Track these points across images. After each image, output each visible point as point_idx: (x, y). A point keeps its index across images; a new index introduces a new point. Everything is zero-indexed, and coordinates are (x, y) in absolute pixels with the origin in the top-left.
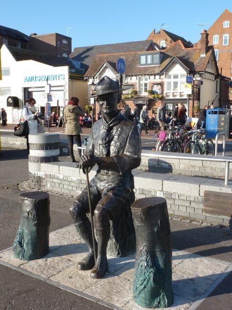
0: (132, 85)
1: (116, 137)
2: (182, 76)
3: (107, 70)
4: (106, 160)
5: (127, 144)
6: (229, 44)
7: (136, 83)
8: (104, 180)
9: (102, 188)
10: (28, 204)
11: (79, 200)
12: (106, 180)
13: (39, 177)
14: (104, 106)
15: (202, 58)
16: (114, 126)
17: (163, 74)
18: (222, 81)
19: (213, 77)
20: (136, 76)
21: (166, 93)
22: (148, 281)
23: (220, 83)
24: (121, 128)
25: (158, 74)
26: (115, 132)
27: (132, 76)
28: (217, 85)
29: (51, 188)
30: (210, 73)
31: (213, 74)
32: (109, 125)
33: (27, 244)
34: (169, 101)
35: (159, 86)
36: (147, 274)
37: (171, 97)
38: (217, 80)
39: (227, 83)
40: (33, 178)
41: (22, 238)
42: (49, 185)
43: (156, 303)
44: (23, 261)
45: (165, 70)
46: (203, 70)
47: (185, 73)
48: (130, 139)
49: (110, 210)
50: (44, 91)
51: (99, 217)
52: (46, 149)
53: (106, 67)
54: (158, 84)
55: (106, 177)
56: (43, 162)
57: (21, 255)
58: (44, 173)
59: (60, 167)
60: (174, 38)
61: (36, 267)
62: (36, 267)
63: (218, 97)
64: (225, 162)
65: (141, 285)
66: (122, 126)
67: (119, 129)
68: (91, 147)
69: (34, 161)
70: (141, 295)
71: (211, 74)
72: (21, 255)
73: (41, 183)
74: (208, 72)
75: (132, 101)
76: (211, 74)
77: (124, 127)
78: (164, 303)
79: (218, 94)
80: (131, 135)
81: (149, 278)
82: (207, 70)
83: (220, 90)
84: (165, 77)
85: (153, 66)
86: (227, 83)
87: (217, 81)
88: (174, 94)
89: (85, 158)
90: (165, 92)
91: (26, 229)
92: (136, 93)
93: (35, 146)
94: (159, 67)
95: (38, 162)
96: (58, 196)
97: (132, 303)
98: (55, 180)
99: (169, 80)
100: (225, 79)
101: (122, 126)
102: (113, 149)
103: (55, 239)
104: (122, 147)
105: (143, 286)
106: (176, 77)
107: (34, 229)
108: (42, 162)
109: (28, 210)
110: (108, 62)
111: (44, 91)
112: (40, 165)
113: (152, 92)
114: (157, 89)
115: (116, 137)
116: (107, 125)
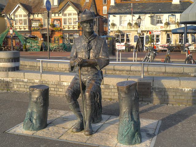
0: (39, 20)
1: (94, 47)
2: (74, 14)
3: (20, 9)
4: (88, 60)
5: (101, 51)
7: (42, 19)
8: (86, 75)
9: (85, 79)
10: (36, 94)
11: (71, 88)
12: (87, 74)
13: (7, 82)
15: (87, 2)
16: (92, 40)
17: (61, 13)
20: (41, 14)
22: (130, 129)
23: (99, 20)
25: (57, 13)
26: (93, 44)
27: (39, 14)
29: (18, 89)
32: (89, 39)
33: (36, 120)
34: (72, 32)
35: (59, 22)
36: (129, 125)
37: (67, 29)
39: (103, 20)
40: (2, 83)
41: (31, 115)
42: (15, 87)
43: (134, 141)
44: (34, 132)
45: (62, 10)
47: (76, 12)
48: (103, 48)
49: (94, 92)
51: (89, 96)
52: (12, 62)
53: (19, 7)
54: (57, 20)
55: (87, 72)
56: (10, 71)
57: (31, 128)
58: (11, 79)
59: (25, 74)
61: (41, 133)
62: (41, 133)
63: (98, 29)
64: (142, 64)
65: (125, 132)
66: (97, 40)
67: (96, 42)
68: (75, 54)
69: (3, 71)
70: (126, 138)
72: (31, 128)
73: (8, 86)
75: (39, 32)
77: (99, 41)
78: (138, 141)
79: (98, 27)
80: (103, 46)
81: (131, 127)
83: (99, 25)
84: (63, 15)
85: (54, 7)
86: (103, 20)
88: (74, 27)
89: (79, 60)
90: (62, 26)
91: (34, 110)
92: (41, 26)
93: (3, 60)
94: (58, 8)
95: (6, 71)
96: (25, 94)
97: (119, 144)
98: (20, 83)
99: (65, 17)
101: (97, 40)
102: (91, 55)
103: (52, 114)
104: (98, 53)
105: (127, 133)
106: (70, 14)
107: (42, 109)
108: (9, 71)
109: (37, 97)
110: (20, 3)
112: (8, 74)
113: (54, 26)
114: (56, 23)
115: (94, 47)
116: (87, 39)
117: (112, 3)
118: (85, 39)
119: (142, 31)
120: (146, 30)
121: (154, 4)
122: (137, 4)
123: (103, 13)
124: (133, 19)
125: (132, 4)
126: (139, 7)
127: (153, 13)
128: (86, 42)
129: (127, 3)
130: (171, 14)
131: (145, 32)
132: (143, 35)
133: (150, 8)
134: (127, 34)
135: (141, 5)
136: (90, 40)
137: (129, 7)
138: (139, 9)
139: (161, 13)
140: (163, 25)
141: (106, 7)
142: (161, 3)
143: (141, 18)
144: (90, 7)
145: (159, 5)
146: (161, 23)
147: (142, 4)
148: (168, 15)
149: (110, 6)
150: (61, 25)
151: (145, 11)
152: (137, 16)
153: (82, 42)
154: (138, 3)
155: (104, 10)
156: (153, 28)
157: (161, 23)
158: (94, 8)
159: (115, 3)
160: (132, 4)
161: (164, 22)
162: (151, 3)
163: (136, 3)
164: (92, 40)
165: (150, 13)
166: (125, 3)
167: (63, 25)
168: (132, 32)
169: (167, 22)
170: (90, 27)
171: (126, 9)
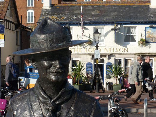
6: (35, 4)
14: (127, 73)
16: (62, 103)
18: (23, 32)
19: (12, 26)
21: (152, 59)
23: (21, 34)
24: (76, 107)
28: (17, 36)
30: (9, 21)
31: (13, 23)
32: (54, 101)
38: (17, 30)
46: (3, 18)
50: (22, 16)
60: (108, 1)
71: (11, 22)
74: (7, 21)
76: (11, 22)
82: (6, 18)
87: (17, 32)
100: (27, 30)
111: (22, 16)
117: (46, 5)
118: (41, 99)
119: (101, 56)
120: (107, 52)
121: (118, 8)
122: (90, 8)
124: (84, 34)
125: (81, 7)
126: (93, 13)
127: (118, 24)
128: (48, 110)
129: (71, 5)
130: (149, 26)
131: (105, 56)
132: (102, 61)
133: (113, 15)
134: (74, 59)
135: (97, 9)
136: (57, 103)
137: (76, 12)
138: (93, 16)
139: (132, 23)
140: (136, 44)
141: (33, 11)
142: (131, 6)
143: (99, 30)
144: (6, 10)
145: (127, 9)
146: (133, 40)
147: (99, 7)
148: (144, 26)
149: (43, 10)
151: (105, 19)
152: (91, 29)
153: (35, 108)
154: (92, 6)
155: (29, 17)
156: (119, 50)
157: (133, 40)
158: (13, 12)
159: (52, 5)
160: (81, 7)
161: (138, 39)
162: (115, 6)
163: (87, 6)
164: (62, 103)
165: (112, 23)
166: (68, 5)
168: (82, 56)
169: (142, 40)
170: (59, 68)
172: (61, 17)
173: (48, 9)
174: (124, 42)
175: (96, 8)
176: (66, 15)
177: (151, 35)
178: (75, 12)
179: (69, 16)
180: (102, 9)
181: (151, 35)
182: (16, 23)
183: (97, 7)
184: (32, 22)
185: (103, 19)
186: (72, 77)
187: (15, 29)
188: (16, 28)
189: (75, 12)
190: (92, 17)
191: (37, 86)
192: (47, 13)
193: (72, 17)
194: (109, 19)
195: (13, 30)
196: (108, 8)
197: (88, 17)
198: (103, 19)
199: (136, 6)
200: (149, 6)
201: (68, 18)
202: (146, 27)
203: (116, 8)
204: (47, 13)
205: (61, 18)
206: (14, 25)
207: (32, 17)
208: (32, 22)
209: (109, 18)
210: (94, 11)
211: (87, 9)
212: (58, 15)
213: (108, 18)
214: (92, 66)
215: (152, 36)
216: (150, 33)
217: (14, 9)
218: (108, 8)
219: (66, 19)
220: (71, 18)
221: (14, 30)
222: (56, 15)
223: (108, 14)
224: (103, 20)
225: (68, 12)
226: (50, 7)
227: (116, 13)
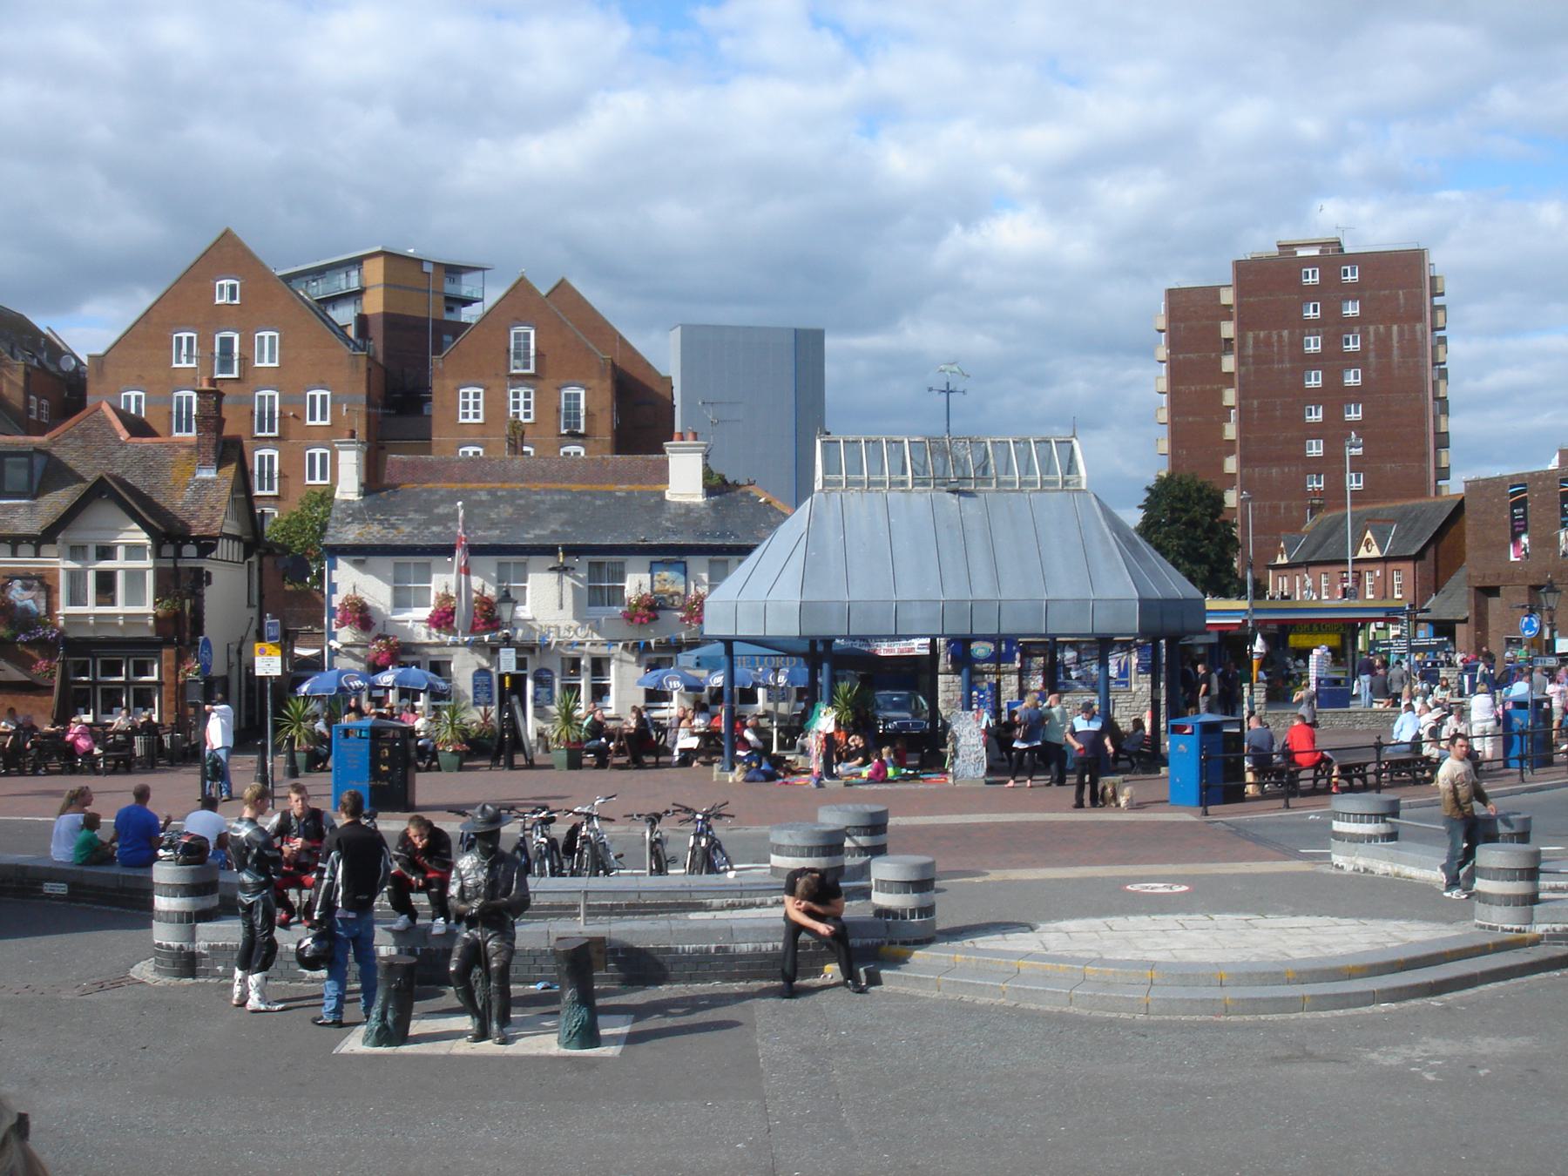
83: (261, 597)
123: (532, 370)
138: (493, 525)
150: (51, 607)
167: (64, 609)
171: (427, 524)
172: (393, 526)
173: (353, 501)
174: (590, 605)
175: (503, 496)
176: (411, 520)
177: (667, 587)
178: (436, 511)
179: (420, 525)
180: (522, 502)
181: (667, 587)
182: (247, 537)
183: (504, 493)
184: (273, 431)
185: (526, 536)
186: (1477, 660)
187: (245, 558)
188: (247, 554)
189: (436, 511)
190: (490, 529)
191: (519, 505)
192: (350, 515)
193: (428, 529)
194: (542, 537)
195: (238, 562)
196: (538, 497)
197: (479, 529)
198: (526, 536)
199: (623, 494)
200: (662, 494)
201: (416, 532)
202: (652, 563)
203: (563, 497)
204: (350, 515)
205: (395, 532)
206: (242, 544)
207: (272, 413)
208: (273, 431)
209: (543, 532)
210: (497, 507)
211: (475, 501)
212: (386, 520)
213: (537, 532)
214: (490, 680)
215: (671, 590)
216: (665, 580)
217: (243, 496)
218: (538, 497)
219: (410, 535)
220: (426, 532)
221: (241, 560)
222: (381, 522)
223: (537, 520)
224: (525, 540)
225: (416, 511)
226: (359, 496)
227: (564, 516)
